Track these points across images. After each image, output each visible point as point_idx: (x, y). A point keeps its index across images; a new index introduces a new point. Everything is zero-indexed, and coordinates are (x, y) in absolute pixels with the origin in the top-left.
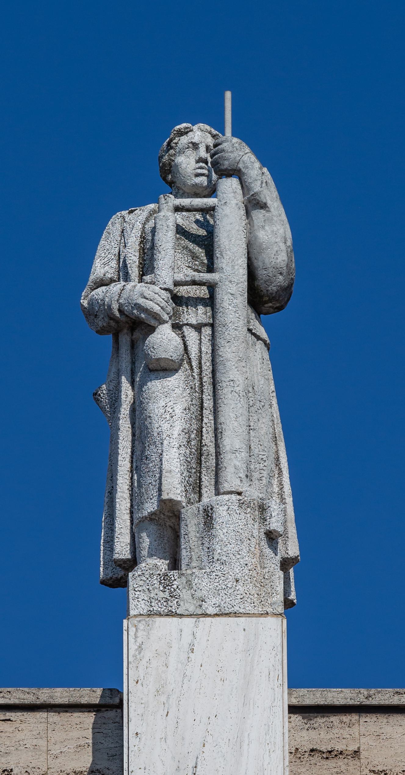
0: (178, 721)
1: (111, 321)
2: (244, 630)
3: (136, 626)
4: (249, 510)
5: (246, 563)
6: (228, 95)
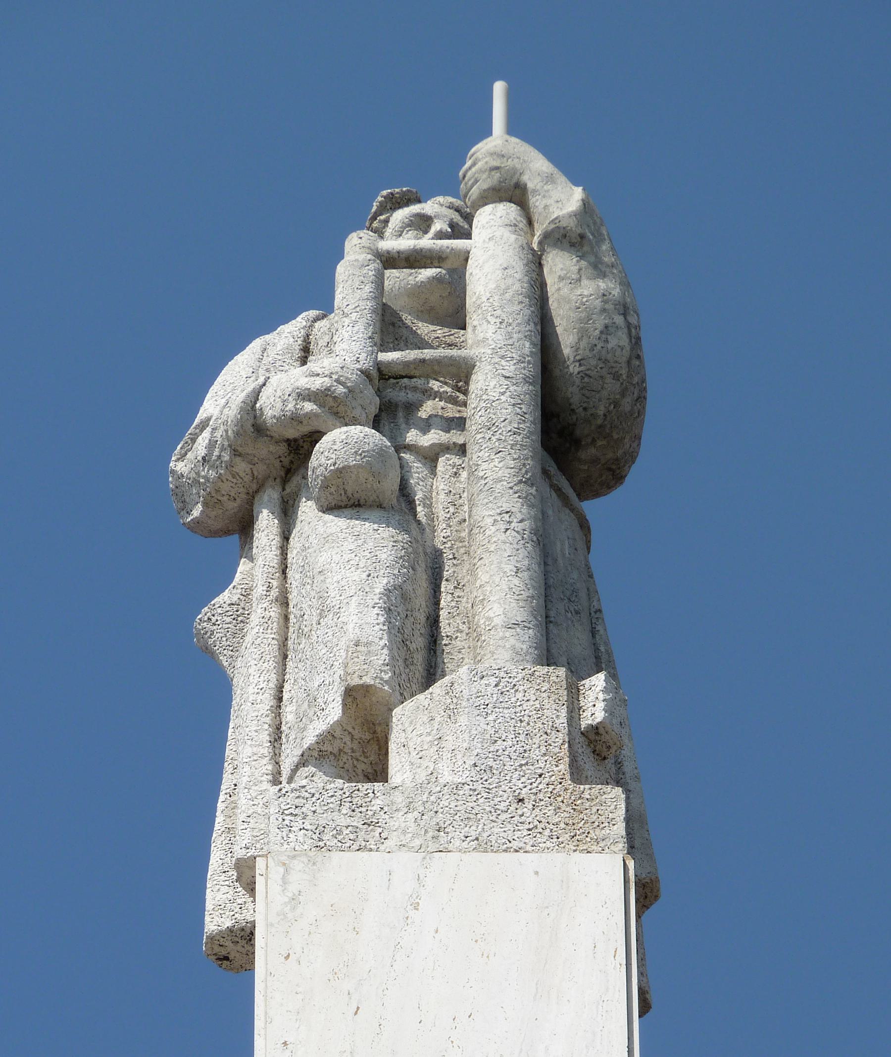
0: (382, 1022)
1: (238, 460)
2: (537, 873)
3: (284, 864)
4: (546, 686)
5: (540, 771)
6: (499, 88)
